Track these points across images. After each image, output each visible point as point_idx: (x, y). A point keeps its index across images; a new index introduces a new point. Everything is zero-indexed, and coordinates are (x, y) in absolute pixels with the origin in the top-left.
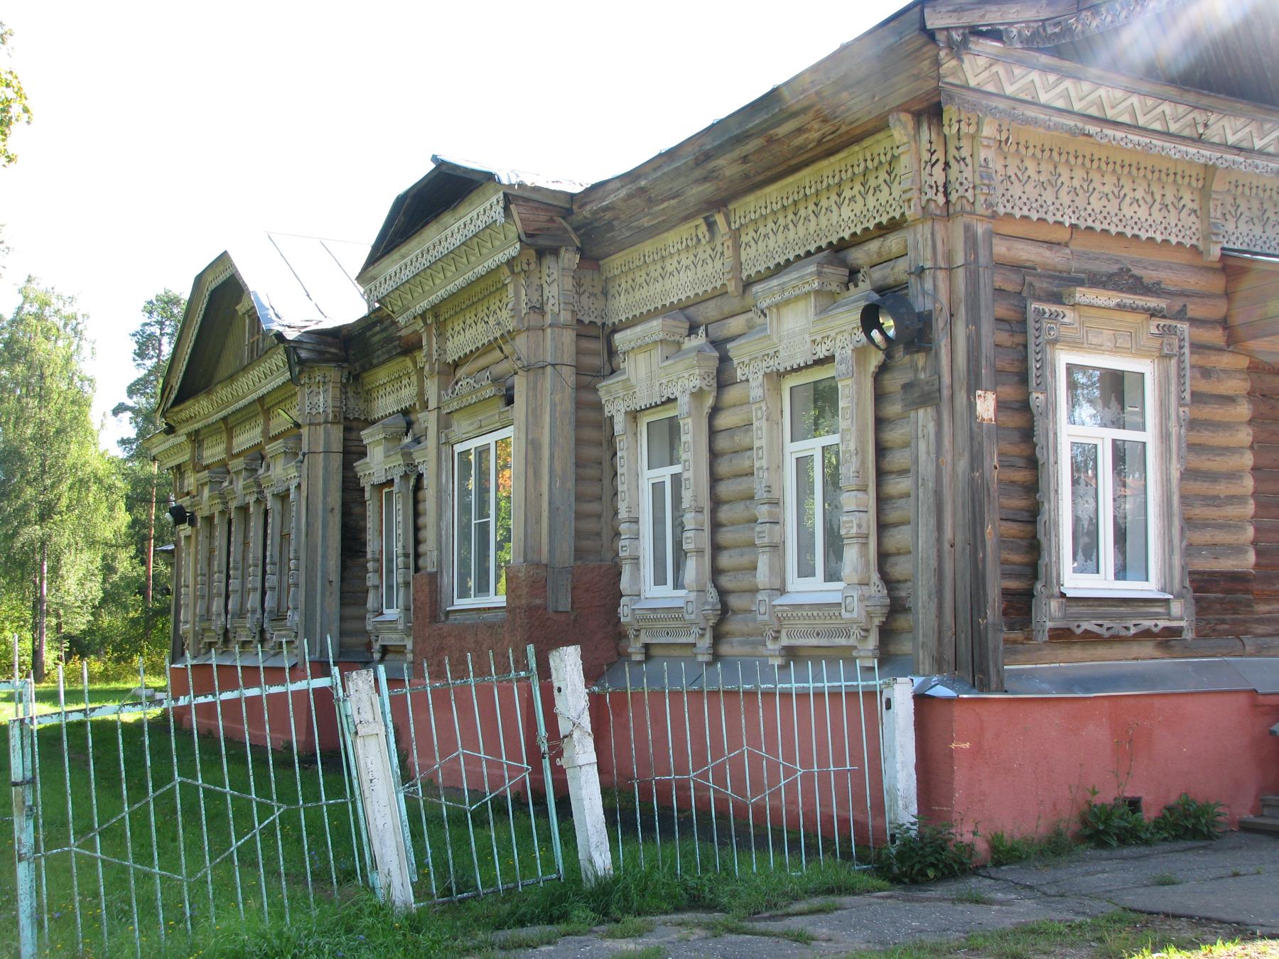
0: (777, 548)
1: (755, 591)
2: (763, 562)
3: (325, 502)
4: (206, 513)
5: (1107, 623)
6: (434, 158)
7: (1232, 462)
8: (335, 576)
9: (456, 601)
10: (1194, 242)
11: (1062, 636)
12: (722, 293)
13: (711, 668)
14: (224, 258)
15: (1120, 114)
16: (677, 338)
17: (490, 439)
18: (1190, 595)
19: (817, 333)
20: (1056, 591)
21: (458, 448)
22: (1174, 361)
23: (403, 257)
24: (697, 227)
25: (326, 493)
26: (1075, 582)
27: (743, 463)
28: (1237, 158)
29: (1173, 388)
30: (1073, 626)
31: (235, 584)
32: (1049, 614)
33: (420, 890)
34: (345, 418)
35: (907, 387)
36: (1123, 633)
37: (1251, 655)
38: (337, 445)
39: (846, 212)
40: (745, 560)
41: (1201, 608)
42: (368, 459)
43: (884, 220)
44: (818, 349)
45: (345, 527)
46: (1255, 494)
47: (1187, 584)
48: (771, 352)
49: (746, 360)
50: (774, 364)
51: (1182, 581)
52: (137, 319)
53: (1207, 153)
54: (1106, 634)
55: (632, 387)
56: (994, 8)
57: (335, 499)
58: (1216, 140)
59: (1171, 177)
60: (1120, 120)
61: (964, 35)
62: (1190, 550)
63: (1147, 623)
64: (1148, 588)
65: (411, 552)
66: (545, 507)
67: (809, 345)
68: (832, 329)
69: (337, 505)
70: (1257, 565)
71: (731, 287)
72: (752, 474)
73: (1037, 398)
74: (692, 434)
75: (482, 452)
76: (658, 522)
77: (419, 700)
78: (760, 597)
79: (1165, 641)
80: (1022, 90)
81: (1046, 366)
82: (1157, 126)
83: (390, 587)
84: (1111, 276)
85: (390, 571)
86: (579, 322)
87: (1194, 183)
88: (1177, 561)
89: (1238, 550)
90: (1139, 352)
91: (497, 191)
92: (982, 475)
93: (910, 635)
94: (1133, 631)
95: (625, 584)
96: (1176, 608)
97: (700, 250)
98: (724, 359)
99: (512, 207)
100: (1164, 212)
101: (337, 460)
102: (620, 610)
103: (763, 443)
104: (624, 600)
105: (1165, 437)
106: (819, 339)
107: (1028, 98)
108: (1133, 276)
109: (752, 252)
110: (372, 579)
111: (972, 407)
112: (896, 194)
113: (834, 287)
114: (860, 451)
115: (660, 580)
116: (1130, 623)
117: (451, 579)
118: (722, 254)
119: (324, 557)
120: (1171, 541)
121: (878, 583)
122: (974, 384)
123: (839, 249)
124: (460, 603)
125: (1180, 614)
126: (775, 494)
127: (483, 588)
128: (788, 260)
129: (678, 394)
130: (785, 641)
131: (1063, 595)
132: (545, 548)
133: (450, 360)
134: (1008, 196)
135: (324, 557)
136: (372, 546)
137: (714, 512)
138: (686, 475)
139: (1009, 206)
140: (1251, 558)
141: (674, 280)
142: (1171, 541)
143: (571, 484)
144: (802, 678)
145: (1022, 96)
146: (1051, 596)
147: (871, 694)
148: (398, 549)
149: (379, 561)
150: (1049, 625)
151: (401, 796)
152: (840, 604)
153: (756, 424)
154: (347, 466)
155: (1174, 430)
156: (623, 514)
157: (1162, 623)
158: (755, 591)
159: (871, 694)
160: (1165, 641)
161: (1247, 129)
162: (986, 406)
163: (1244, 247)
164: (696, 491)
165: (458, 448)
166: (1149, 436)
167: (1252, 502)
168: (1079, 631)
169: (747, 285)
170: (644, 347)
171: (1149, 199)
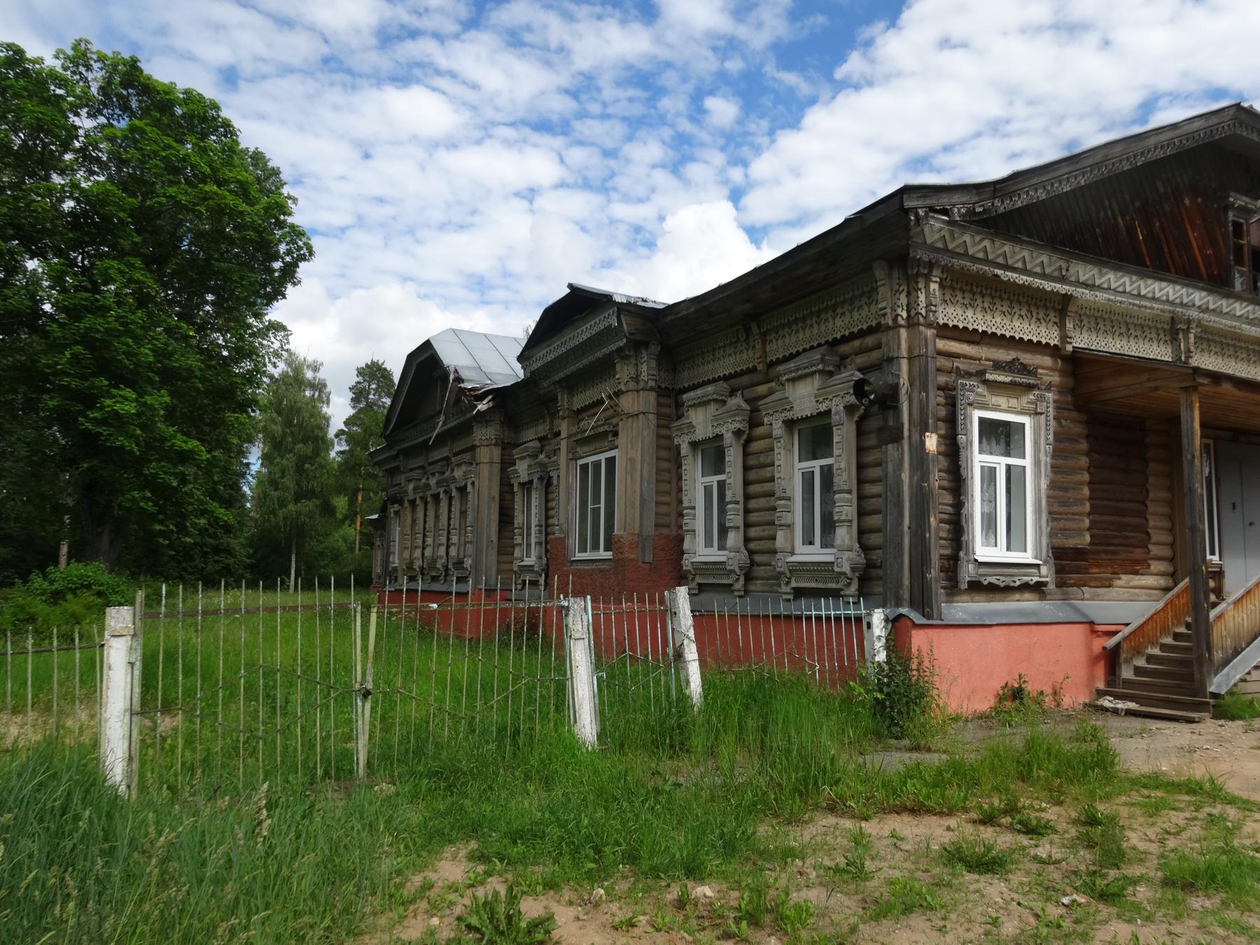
0: (790, 527)
1: (775, 552)
2: (780, 535)
3: (489, 493)
4: (411, 497)
5: (1002, 578)
6: (570, 286)
7: (1078, 477)
8: (494, 538)
9: (577, 554)
10: (1056, 342)
11: (976, 587)
12: (753, 370)
13: (742, 600)
14: (427, 345)
15: (1017, 261)
16: (723, 398)
17: (602, 457)
18: (1052, 561)
19: (820, 396)
20: (971, 557)
21: (580, 462)
22: (1043, 417)
23: (549, 346)
24: (737, 330)
25: (490, 488)
26: (984, 551)
27: (767, 473)
28: (1084, 291)
29: (1043, 433)
30: (982, 579)
31: (429, 541)
32: (968, 573)
33: (601, 736)
34: (503, 443)
35: (880, 430)
36: (1012, 584)
37: (1088, 600)
38: (497, 459)
39: (839, 322)
40: (767, 531)
41: (1059, 571)
42: (516, 467)
43: (865, 327)
44: (820, 406)
45: (501, 508)
46: (1090, 499)
47: (1051, 555)
48: (788, 407)
49: (771, 412)
50: (789, 415)
51: (1048, 552)
52: (354, 379)
53: (1067, 287)
54: (1002, 585)
55: (693, 427)
56: (945, 196)
57: (496, 492)
58: (1073, 279)
59: (1043, 302)
60: (1016, 266)
61: (926, 212)
62: (1052, 535)
63: (1026, 579)
64: (1027, 557)
65: (543, 524)
66: (638, 498)
67: (814, 403)
68: (830, 394)
69: (497, 497)
70: (1091, 544)
71: (760, 367)
72: (773, 481)
73: (962, 439)
74: (734, 457)
75: (597, 465)
76: (708, 508)
77: (607, 616)
78: (779, 556)
79: (1038, 589)
80: (958, 246)
81: (967, 418)
82: (1038, 270)
83: (529, 545)
84: (1008, 363)
85: (529, 535)
86: (659, 387)
87: (1057, 306)
88: (1044, 540)
89: (1079, 532)
90: (1022, 412)
91: (613, 306)
92: (929, 485)
93: (881, 582)
94: (1018, 583)
95: (686, 545)
96: (1044, 570)
97: (739, 346)
98: (755, 410)
99: (622, 316)
100: (1038, 324)
101: (497, 468)
102: (683, 562)
103: (781, 462)
104: (685, 556)
105: (1037, 463)
106: (821, 399)
107: (962, 252)
108: (1021, 364)
109: (774, 346)
110: (518, 540)
111: (923, 443)
112: (873, 311)
113: (831, 368)
114: (848, 468)
115: (708, 543)
116: (1016, 579)
117: (574, 541)
118: (754, 347)
119: (488, 526)
120: (1040, 528)
121: (858, 549)
122: (924, 429)
123: (835, 343)
124: (580, 556)
125: (1046, 574)
126: (788, 494)
127: (595, 547)
128: (798, 351)
129: (724, 432)
130: (794, 584)
131: (976, 560)
132: (637, 524)
133: (575, 409)
134: (945, 313)
135: (488, 526)
136: (519, 519)
137: (745, 504)
138: (728, 481)
139: (946, 319)
140: (1088, 538)
141: (721, 363)
142: (1040, 528)
143: (653, 486)
144: (818, 608)
145: (958, 250)
146: (968, 561)
147: (859, 619)
148: (534, 521)
149: (522, 528)
150: (968, 579)
151: (595, 678)
152: (833, 563)
153: (777, 451)
154: (503, 470)
155: (1043, 458)
156: (685, 504)
157: (1036, 579)
158: (775, 552)
159: (859, 619)
160: (1038, 589)
161: (1091, 273)
162: (931, 442)
163: (1086, 346)
164: (735, 489)
165: (580, 462)
166: (1027, 462)
167: (1088, 504)
168: (986, 583)
169: (772, 365)
170: (704, 403)
171: (1029, 315)
